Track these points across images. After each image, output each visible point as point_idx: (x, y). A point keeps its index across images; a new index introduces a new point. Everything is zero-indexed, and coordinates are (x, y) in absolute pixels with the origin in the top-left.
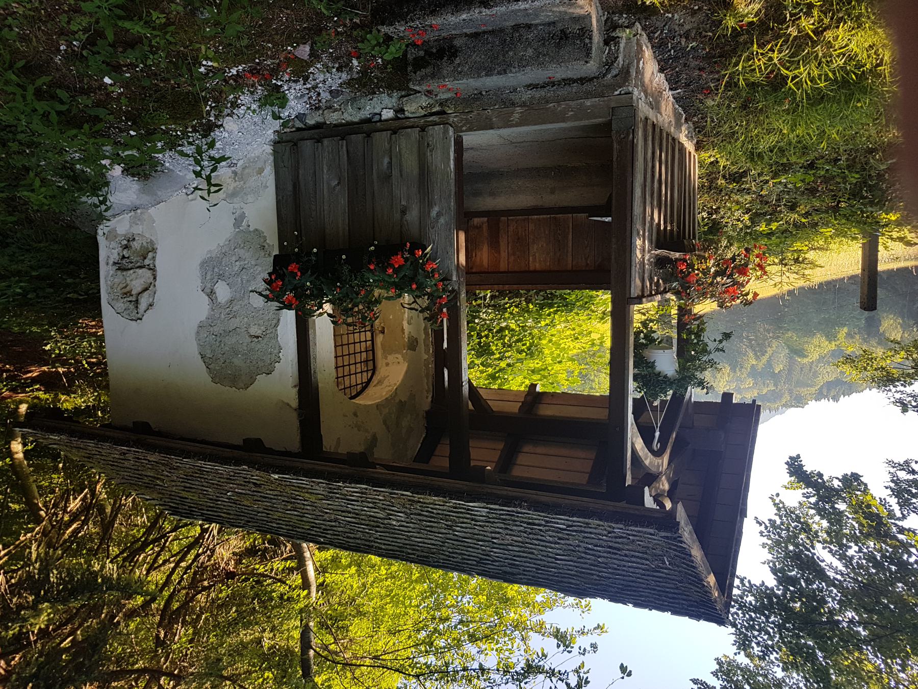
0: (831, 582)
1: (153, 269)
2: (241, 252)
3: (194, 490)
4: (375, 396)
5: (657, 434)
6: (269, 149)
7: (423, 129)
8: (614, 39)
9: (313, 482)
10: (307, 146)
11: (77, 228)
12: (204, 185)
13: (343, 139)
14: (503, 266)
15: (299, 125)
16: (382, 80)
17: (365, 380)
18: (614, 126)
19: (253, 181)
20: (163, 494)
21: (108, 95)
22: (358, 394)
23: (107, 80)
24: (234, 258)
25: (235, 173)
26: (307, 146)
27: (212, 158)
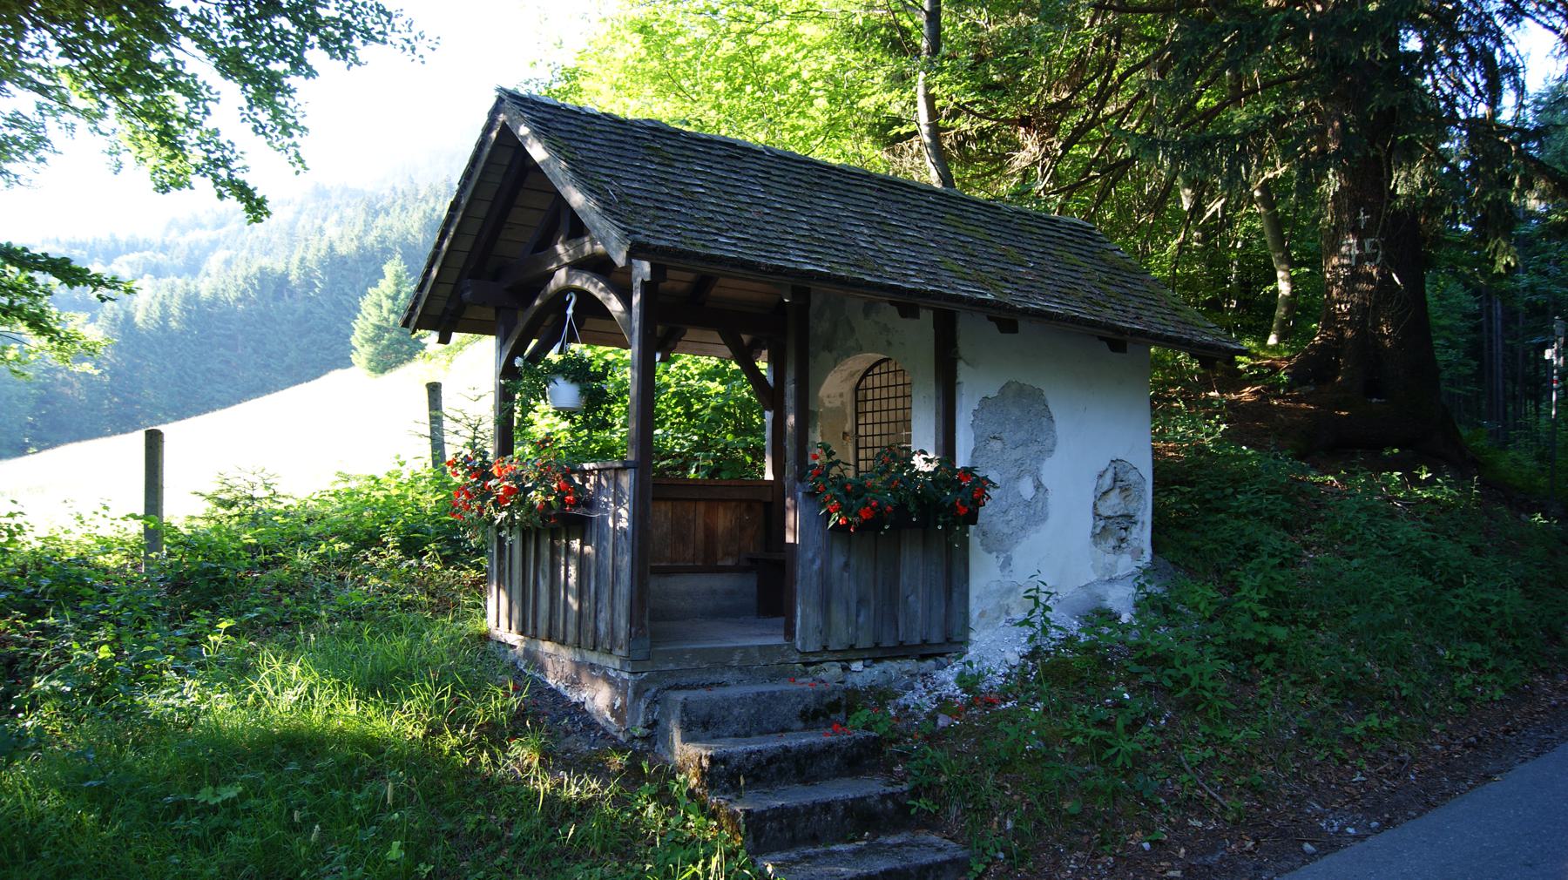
0: (186, 32)
1: (1097, 515)
2: (1006, 530)
3: (1068, 267)
4: (859, 363)
5: (570, 311)
6: (973, 636)
7: (825, 648)
8: (648, 727)
9: (954, 289)
10: (936, 637)
11: (1173, 562)
12: (1043, 597)
13: (902, 643)
14: (701, 507)
15: (943, 660)
16: (863, 698)
17: (869, 379)
18: (648, 642)
19: (990, 604)
20: (1101, 259)
21: (1127, 684)
22: (879, 363)
23: (1126, 696)
24: (1014, 523)
25: (1008, 613)
26: (936, 637)
27: (1032, 625)
